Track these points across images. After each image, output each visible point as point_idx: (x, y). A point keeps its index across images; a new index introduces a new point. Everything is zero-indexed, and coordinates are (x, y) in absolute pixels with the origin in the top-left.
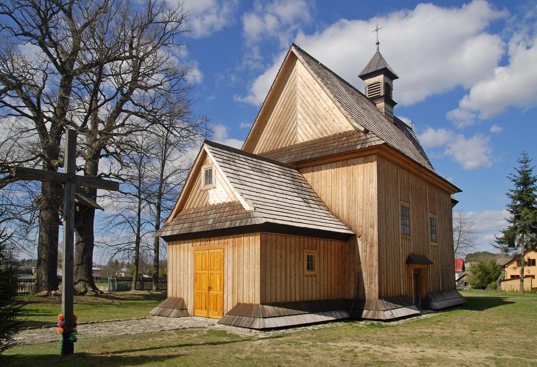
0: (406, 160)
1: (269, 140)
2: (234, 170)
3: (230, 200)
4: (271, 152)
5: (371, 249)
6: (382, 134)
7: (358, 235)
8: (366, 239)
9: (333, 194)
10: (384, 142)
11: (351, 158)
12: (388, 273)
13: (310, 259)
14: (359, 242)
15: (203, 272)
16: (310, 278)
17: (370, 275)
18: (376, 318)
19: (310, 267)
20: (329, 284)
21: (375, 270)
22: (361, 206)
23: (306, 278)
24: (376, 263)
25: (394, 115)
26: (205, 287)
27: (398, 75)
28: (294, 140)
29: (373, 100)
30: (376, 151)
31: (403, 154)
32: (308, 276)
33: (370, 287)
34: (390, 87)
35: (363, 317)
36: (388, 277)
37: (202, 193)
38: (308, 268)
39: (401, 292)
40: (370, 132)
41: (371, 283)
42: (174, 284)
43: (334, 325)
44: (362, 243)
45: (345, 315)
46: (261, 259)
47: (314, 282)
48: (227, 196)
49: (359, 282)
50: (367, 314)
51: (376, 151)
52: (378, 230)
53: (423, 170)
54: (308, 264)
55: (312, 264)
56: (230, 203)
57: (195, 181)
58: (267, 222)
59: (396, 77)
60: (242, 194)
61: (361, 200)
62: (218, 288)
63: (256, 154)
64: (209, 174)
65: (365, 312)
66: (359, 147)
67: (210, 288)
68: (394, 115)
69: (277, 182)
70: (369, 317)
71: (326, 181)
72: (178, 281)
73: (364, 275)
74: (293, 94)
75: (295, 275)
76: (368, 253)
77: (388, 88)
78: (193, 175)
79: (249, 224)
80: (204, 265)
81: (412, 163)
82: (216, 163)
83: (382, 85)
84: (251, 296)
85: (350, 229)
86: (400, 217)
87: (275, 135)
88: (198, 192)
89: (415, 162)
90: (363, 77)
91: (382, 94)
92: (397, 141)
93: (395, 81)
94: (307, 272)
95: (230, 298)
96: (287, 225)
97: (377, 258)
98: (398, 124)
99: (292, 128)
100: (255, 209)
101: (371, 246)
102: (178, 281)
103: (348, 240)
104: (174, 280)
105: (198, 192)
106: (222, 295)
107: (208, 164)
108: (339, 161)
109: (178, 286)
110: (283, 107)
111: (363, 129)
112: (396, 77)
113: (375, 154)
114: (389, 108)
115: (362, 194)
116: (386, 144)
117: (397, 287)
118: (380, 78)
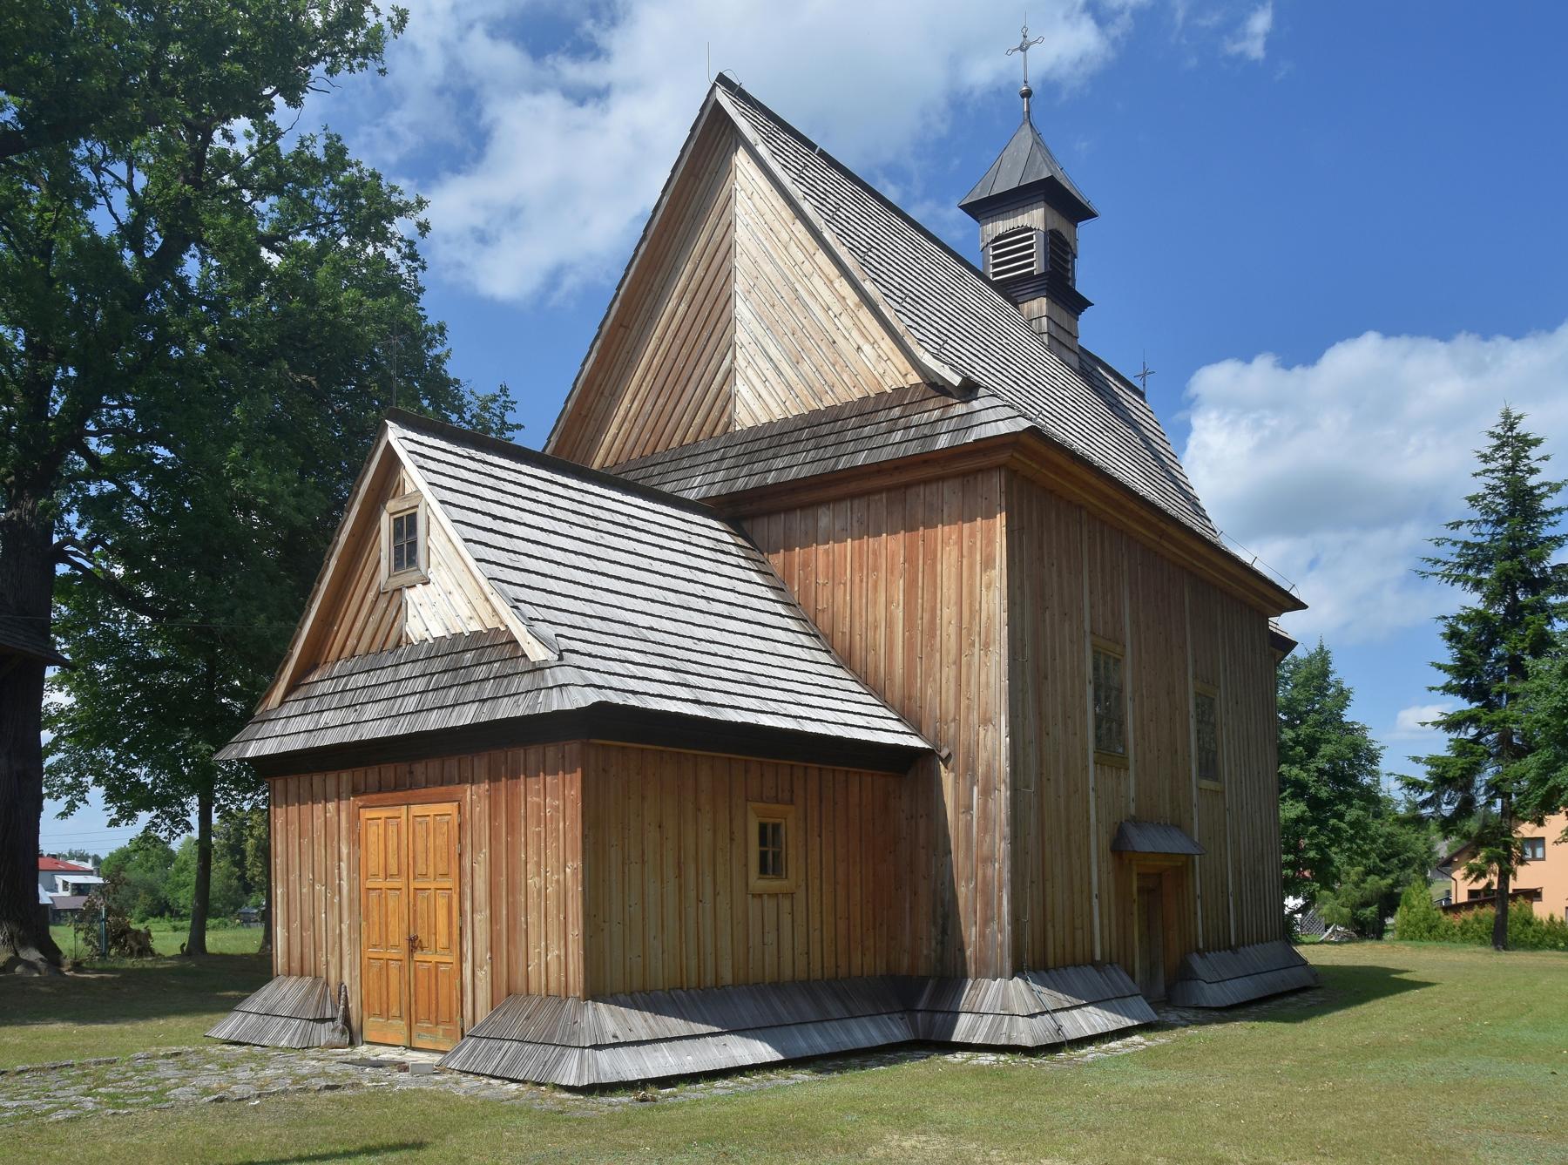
0: (1110, 492)
1: (640, 421)
2: (495, 517)
3: (475, 626)
4: (645, 462)
5: (986, 802)
6: (1021, 388)
7: (944, 753)
8: (970, 768)
9: (856, 608)
10: (1027, 424)
11: (918, 483)
12: (1049, 885)
13: (768, 834)
14: (947, 778)
15: (391, 883)
16: (770, 904)
17: (985, 891)
18: (1003, 1041)
19: (770, 864)
20: (842, 925)
21: (1000, 870)
22: (953, 651)
23: (754, 904)
24: (1002, 848)
25: (1080, 342)
26: (397, 935)
27: (1095, 205)
28: (725, 419)
29: (1012, 290)
30: (1003, 457)
31: (1100, 473)
32: (760, 895)
33: (983, 935)
34: (1067, 244)
35: (957, 1037)
36: (1049, 900)
37: (382, 604)
38: (763, 869)
39: (1092, 952)
40: (982, 392)
41: (987, 921)
42: (296, 925)
43: (778, 1078)
44: (956, 782)
45: (898, 1032)
46: (584, 836)
47: (786, 919)
48: (465, 611)
49: (945, 917)
50: (973, 1029)
51: (1003, 457)
52: (1012, 734)
53: (1171, 530)
54: (763, 856)
55: (776, 856)
56: (475, 635)
57: (360, 556)
58: (600, 703)
59: (1090, 215)
60: (516, 604)
61: (952, 630)
62: (443, 941)
63: (595, 467)
64: (407, 527)
65: (964, 1021)
66: (943, 442)
67: (414, 944)
68: (1080, 342)
69: (657, 566)
70: (978, 1039)
71: (861, 569)
72: (307, 914)
73: (963, 891)
74: (724, 251)
75: (716, 894)
76: (977, 816)
77: (1060, 250)
78: (352, 534)
79: (540, 709)
80: (393, 862)
81: (1132, 505)
82: (429, 495)
83: (1038, 242)
84: (553, 968)
85: (918, 731)
86: (1090, 690)
87: (661, 401)
88: (371, 595)
89: (1143, 501)
90: (982, 210)
91: (1038, 267)
92: (1081, 428)
93: (1084, 228)
94: (757, 883)
95: (483, 975)
96: (677, 714)
97: (1007, 830)
98: (1089, 369)
99: (719, 377)
100: (561, 658)
101: (986, 792)
102: (307, 914)
103: (907, 770)
104: (296, 915)
105: (371, 595)
106: (456, 966)
107: (405, 497)
108: (879, 491)
109: (308, 934)
110: (688, 296)
111: (956, 380)
112: (1090, 215)
113: (999, 467)
114: (1063, 317)
115: (954, 609)
116: (1034, 431)
117: (1079, 933)
118: (1035, 218)
